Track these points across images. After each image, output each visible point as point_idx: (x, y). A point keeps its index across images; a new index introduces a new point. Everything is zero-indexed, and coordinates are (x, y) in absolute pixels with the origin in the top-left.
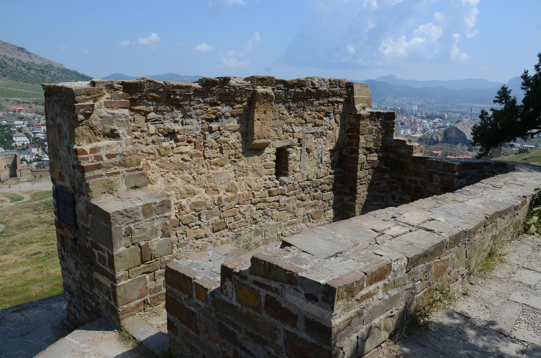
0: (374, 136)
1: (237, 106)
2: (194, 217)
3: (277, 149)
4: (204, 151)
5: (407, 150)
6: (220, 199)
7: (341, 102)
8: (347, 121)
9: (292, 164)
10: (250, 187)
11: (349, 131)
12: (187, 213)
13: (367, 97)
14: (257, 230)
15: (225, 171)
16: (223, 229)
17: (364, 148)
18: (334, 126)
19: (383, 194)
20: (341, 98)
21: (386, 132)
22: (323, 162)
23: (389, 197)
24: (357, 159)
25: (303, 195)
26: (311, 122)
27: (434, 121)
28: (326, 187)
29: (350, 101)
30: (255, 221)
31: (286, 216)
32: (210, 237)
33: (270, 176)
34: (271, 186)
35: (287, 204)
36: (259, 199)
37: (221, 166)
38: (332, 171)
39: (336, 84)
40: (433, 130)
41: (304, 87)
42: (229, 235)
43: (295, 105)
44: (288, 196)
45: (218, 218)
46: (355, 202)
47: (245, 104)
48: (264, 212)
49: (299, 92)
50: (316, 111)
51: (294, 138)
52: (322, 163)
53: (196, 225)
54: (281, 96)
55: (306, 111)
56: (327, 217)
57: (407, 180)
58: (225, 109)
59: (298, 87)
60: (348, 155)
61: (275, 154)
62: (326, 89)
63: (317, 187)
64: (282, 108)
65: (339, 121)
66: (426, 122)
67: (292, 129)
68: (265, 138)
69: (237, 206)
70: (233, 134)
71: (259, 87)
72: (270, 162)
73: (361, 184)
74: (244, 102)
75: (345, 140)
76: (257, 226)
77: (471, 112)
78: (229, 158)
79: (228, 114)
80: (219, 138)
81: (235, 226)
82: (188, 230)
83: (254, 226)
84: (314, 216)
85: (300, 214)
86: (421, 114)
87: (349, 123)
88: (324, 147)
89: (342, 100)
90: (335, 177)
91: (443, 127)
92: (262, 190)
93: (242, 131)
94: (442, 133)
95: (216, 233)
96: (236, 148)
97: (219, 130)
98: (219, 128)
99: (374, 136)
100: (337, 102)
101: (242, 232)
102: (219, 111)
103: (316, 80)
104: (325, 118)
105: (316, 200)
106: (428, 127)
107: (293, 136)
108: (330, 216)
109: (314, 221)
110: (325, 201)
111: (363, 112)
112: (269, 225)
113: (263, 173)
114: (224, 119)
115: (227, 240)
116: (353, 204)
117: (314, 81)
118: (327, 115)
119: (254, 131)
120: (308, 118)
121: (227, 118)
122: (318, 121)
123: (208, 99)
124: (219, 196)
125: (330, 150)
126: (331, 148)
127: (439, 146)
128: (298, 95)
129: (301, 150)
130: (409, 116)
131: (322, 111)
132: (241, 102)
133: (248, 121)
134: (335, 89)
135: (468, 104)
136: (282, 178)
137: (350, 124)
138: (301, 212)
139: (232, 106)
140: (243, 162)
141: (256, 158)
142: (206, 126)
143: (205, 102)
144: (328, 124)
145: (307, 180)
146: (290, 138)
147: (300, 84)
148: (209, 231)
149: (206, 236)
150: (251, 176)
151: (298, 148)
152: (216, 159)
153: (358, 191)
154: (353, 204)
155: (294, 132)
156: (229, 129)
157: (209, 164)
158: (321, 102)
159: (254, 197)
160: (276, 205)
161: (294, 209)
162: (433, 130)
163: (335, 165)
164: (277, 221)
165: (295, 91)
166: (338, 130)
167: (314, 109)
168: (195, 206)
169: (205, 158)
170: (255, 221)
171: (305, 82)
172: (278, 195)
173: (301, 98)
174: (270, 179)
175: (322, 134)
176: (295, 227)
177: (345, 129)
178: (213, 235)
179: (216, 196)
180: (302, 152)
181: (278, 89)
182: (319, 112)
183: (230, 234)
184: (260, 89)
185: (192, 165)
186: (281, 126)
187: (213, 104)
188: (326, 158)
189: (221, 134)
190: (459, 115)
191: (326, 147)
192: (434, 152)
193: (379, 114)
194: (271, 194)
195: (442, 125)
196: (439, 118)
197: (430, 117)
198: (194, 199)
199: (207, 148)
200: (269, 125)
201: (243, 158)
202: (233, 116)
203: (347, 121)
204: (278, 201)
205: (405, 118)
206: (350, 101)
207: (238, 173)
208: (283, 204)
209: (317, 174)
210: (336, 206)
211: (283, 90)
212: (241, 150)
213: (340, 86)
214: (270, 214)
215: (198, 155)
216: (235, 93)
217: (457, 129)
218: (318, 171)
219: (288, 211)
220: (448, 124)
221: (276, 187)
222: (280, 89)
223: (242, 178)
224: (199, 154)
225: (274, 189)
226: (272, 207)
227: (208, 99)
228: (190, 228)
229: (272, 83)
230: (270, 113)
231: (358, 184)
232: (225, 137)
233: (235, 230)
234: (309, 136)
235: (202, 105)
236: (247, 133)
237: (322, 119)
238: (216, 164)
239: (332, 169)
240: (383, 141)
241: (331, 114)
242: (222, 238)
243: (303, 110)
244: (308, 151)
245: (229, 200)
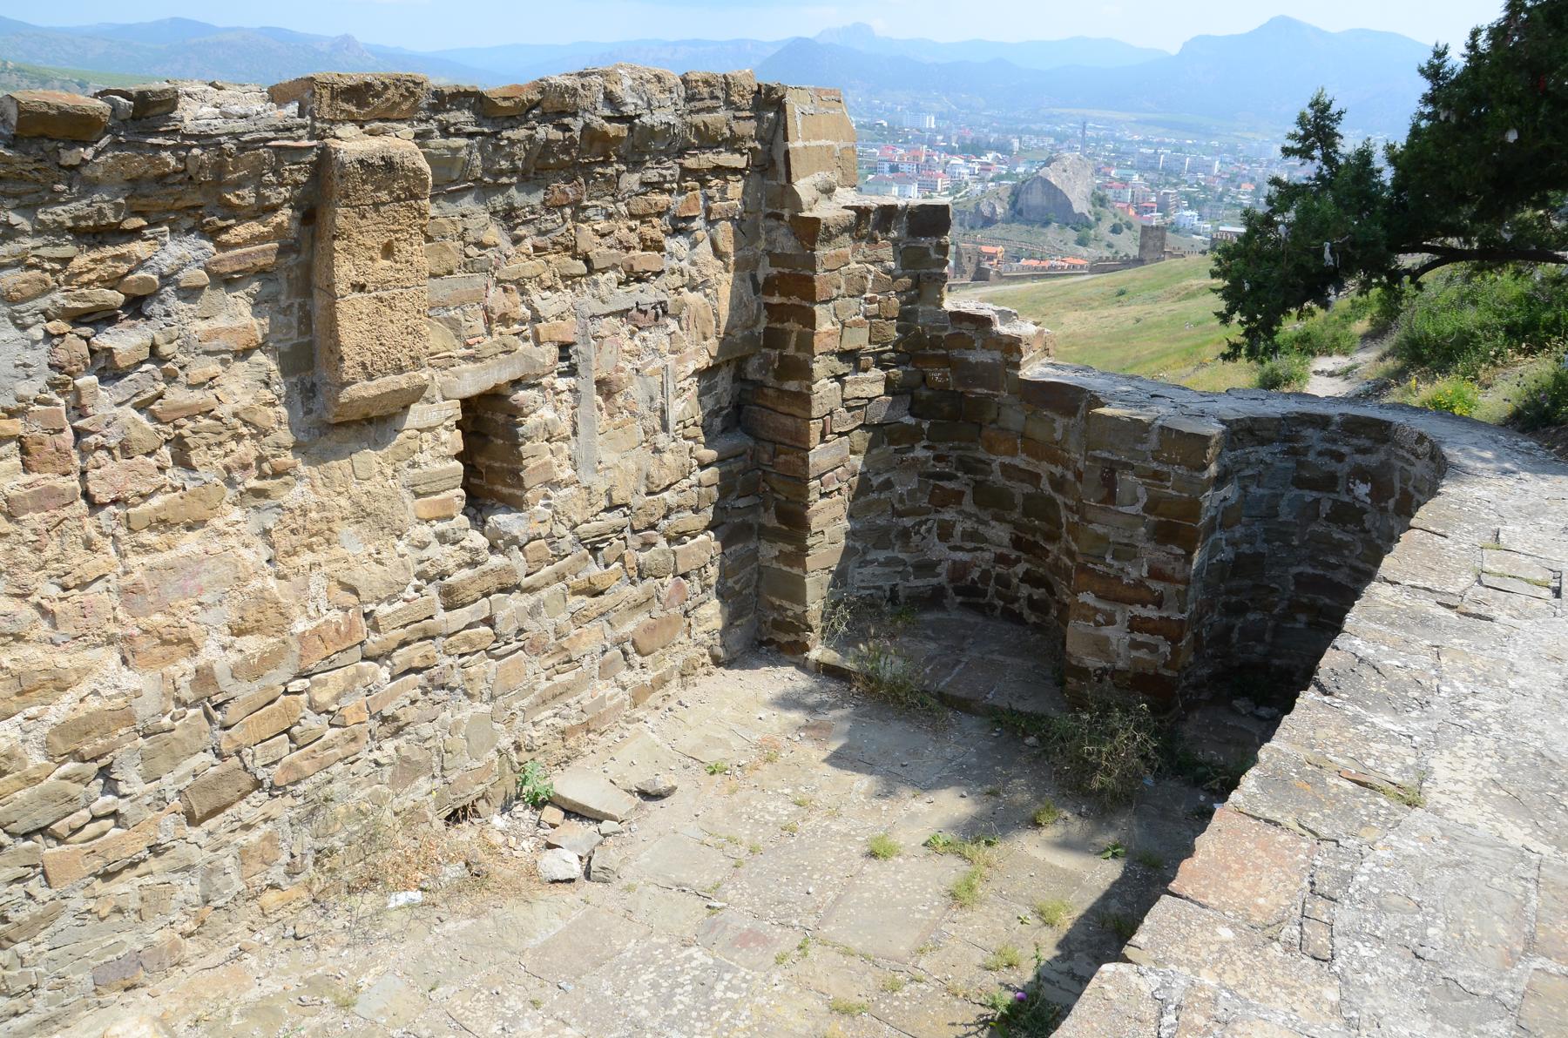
0: (870, 301)
1: (242, 231)
2: (75, 789)
3: (466, 403)
4: (83, 473)
5: (998, 355)
6: (204, 677)
7: (735, 171)
8: (762, 245)
9: (537, 456)
10: (354, 591)
11: (769, 286)
12: (35, 781)
13: (838, 145)
14: (405, 760)
15: (216, 546)
16: (242, 797)
17: (832, 353)
18: (710, 271)
19: (908, 522)
20: (734, 151)
21: (917, 283)
22: (672, 425)
23: (929, 531)
24: (804, 399)
25: (594, 571)
26: (614, 267)
27: (984, 159)
28: (688, 520)
29: (773, 163)
30: (394, 726)
31: (530, 669)
32: (182, 848)
33: (440, 526)
34: (450, 564)
35: (528, 624)
36: (401, 634)
37: (189, 528)
38: (710, 454)
39: (713, 97)
40: (979, 187)
41: (575, 115)
42: (274, 813)
43: (536, 199)
44: (531, 590)
45: (210, 757)
46: (803, 565)
47: (284, 216)
48: (431, 680)
49: (548, 142)
50: (632, 216)
51: (538, 343)
52: (665, 428)
53: (95, 819)
54: (466, 164)
55: (588, 219)
56: (699, 632)
57: (995, 466)
58: (176, 252)
59: (544, 119)
60: (771, 381)
61: (459, 425)
62: (673, 120)
63: (653, 527)
64: (477, 216)
65: (730, 249)
66: (961, 162)
67: (530, 307)
68: (400, 370)
69: (296, 685)
70: (240, 367)
71: (350, 130)
72: (439, 466)
73: (822, 495)
74: (274, 209)
75: (756, 322)
76: (401, 742)
77: (1083, 133)
78: (230, 482)
79: (194, 275)
80: (160, 396)
81: (299, 770)
82: (50, 851)
83: (389, 746)
84: (644, 644)
85: (585, 649)
86: (947, 138)
87: (769, 253)
88: (671, 365)
89: (739, 161)
90: (722, 476)
91: (1009, 176)
92: (410, 593)
93: (285, 347)
94: (1005, 195)
95: (210, 824)
96: (261, 433)
97: (154, 354)
98: (154, 348)
99: (870, 301)
100: (719, 171)
101: (336, 787)
102: (141, 264)
103: (628, 82)
104: (671, 244)
105: (650, 581)
106: (967, 178)
107: (536, 335)
108: (709, 626)
109: (648, 659)
110: (685, 576)
111: (827, 211)
112: (457, 725)
113: (410, 517)
114: (174, 303)
115: (270, 838)
116: (796, 571)
117: (617, 90)
118: (680, 226)
119: (338, 343)
120: (601, 252)
121: (190, 293)
122: (643, 260)
123: (62, 213)
124: (201, 661)
125: (697, 373)
126: (703, 361)
127: (997, 231)
128: (545, 149)
129: (574, 391)
130: (912, 145)
131: (659, 215)
132: (264, 210)
133: (310, 295)
134: (707, 117)
135: (1074, 111)
136: (501, 520)
137: (776, 259)
138: (591, 638)
139: (212, 234)
140: (305, 489)
141: (368, 458)
142: (74, 345)
143: (41, 230)
144: (684, 264)
145: (606, 510)
146: (523, 347)
147: (552, 104)
148: (168, 826)
149: (155, 850)
150: (353, 544)
151: (562, 384)
152: (156, 501)
153: (815, 524)
154: (796, 571)
155: (536, 318)
156: (212, 345)
157: (121, 532)
158: (652, 175)
159: (375, 628)
160: (482, 637)
161: (559, 634)
162: (979, 187)
163: (718, 422)
164: (493, 698)
165: (530, 138)
166: (724, 283)
167: (623, 208)
168: (70, 742)
169: (94, 506)
170: (394, 726)
171: (574, 92)
172: (487, 595)
173: (561, 166)
174: (442, 538)
175: (662, 310)
176: (571, 701)
177: (754, 278)
178: (194, 833)
179: (184, 667)
180: (577, 400)
181: (445, 131)
182: (643, 218)
183: (282, 808)
184: (352, 143)
185: (24, 551)
186: (478, 298)
187: (96, 235)
188: (685, 406)
189: (170, 378)
190: (1052, 141)
191: (679, 362)
192: (985, 249)
193: (888, 214)
194: (452, 600)
195: (1004, 170)
196: (997, 150)
197: (972, 149)
198: (62, 709)
199: (101, 455)
200: (413, 312)
201: (303, 469)
202: (226, 281)
203: (762, 245)
204: (489, 621)
205: (901, 151)
206: (771, 165)
207: (284, 541)
208: (511, 629)
209: (648, 477)
210: (730, 583)
211: (470, 135)
212: (286, 437)
213: (729, 104)
214: (456, 679)
215: (46, 498)
216: (219, 169)
217: (1046, 183)
218: (650, 463)
219: (536, 649)
220: (1020, 170)
221: (473, 564)
222: (458, 134)
223: (307, 558)
224: (52, 493)
225: (466, 573)
226: (465, 649)
227: (62, 213)
228: (60, 840)
229: (415, 108)
230: (416, 252)
231: (814, 496)
232: (191, 387)
233: (301, 788)
234: (605, 326)
235: (29, 243)
236: (307, 358)
237: (661, 249)
238: (162, 524)
239: (707, 445)
240: (905, 317)
241: (694, 225)
242: (241, 838)
243: (574, 216)
244: (605, 388)
245: (251, 670)
